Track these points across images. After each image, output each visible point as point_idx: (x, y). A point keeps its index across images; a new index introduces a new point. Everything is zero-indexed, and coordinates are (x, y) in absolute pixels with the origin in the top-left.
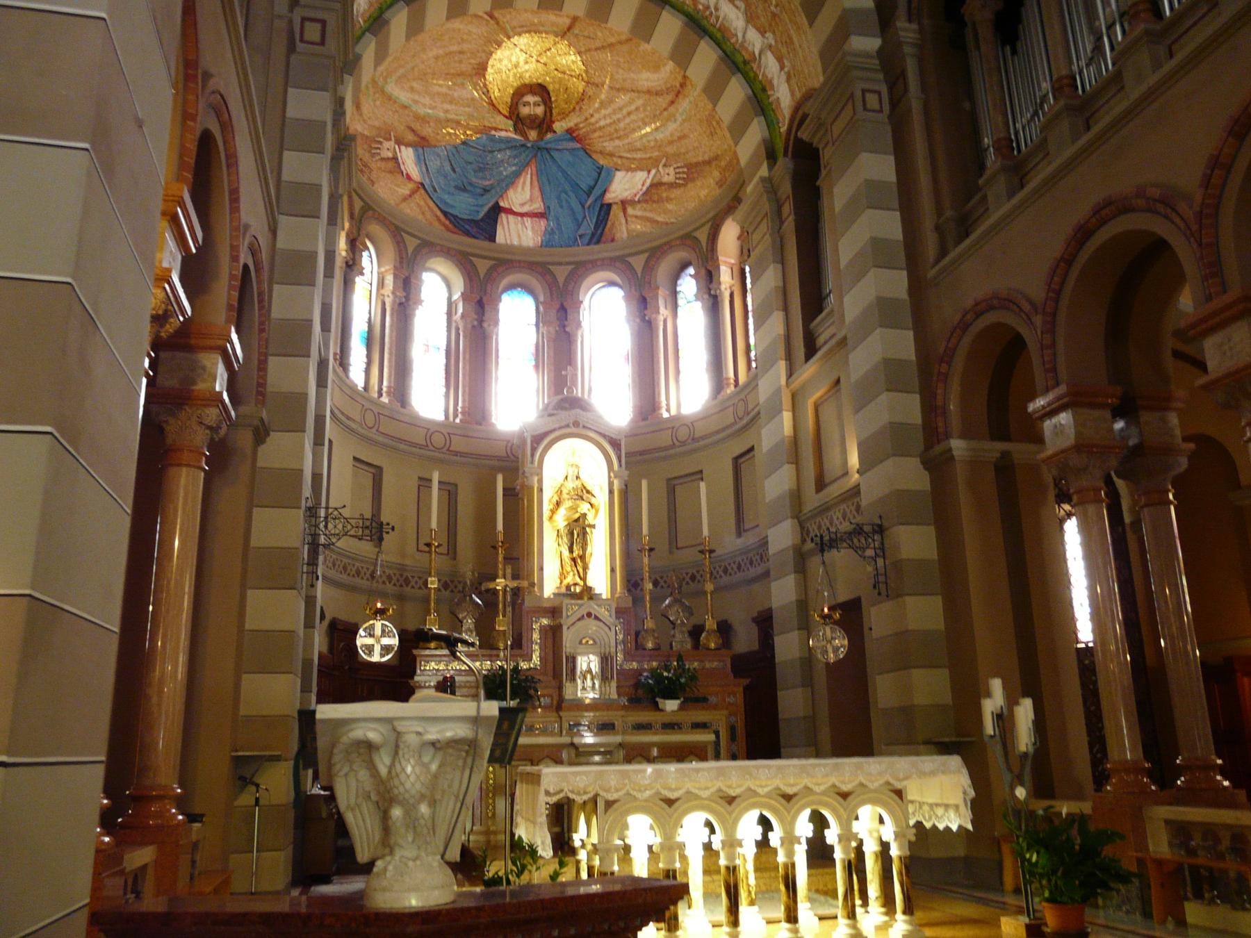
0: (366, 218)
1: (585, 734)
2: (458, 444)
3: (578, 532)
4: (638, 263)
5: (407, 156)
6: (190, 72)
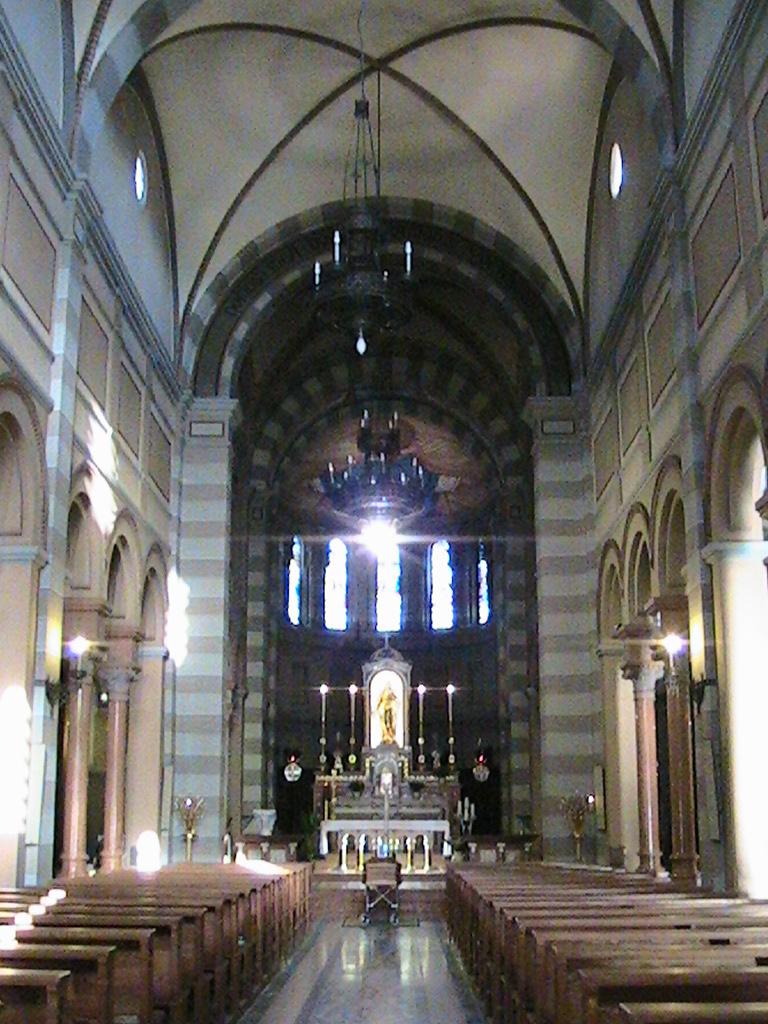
3: (388, 718)
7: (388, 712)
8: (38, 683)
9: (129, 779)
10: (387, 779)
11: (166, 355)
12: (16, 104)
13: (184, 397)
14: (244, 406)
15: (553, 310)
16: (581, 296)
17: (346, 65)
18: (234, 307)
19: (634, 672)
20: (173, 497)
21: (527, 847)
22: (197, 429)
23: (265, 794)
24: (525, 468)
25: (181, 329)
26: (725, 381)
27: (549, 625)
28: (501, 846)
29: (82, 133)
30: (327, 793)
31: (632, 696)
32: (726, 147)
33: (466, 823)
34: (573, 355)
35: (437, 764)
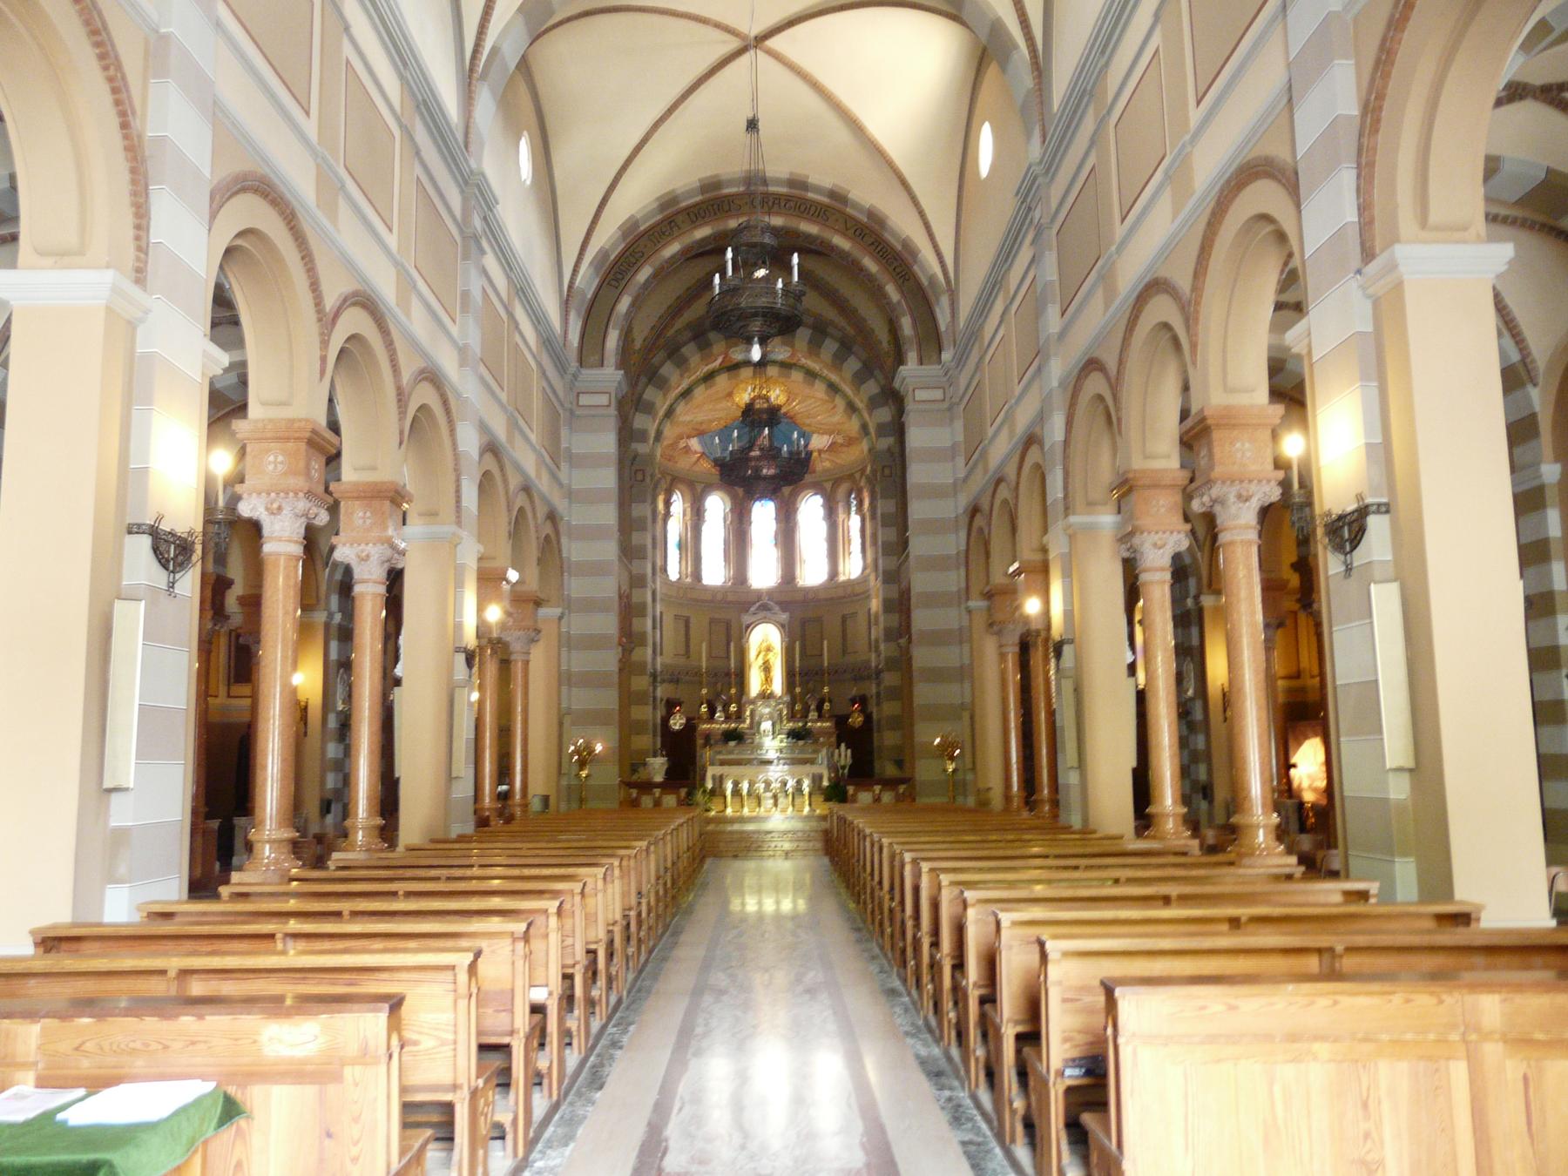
0: (674, 481)
1: (616, 888)
2: (730, 598)
3: (767, 668)
4: (828, 485)
5: (694, 444)
6: (504, 788)
9: (556, 734)
15: (925, 282)
16: (952, 275)
17: (724, 42)
18: (617, 280)
21: (902, 788)
25: (566, 305)
28: (877, 788)
33: (843, 768)
34: (943, 328)
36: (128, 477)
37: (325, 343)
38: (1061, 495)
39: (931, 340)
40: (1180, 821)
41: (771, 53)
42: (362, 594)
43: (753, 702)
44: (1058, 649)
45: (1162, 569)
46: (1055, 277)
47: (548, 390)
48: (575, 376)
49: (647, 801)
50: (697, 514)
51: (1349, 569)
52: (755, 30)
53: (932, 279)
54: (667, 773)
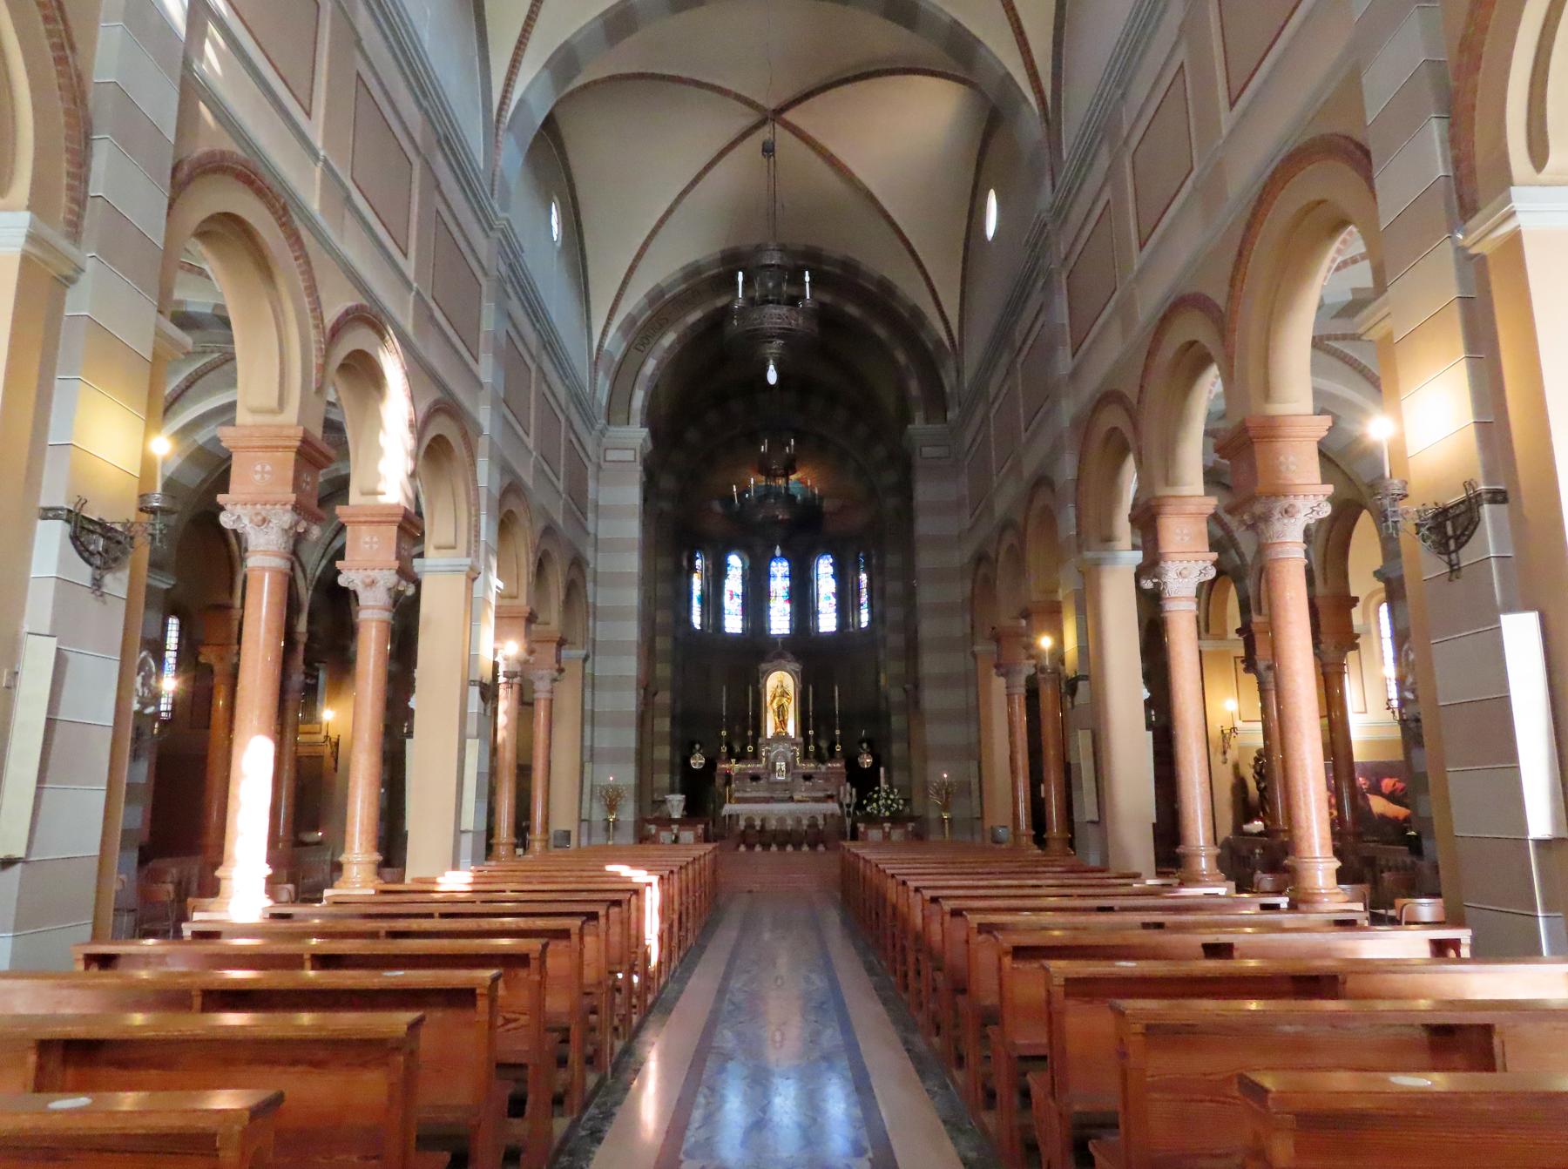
3: (781, 712)
7: (781, 706)
8: (472, 683)
10: (781, 765)
11: (582, 388)
12: (439, 141)
13: (598, 427)
14: (654, 435)
19: (1004, 669)
20: (590, 516)
21: (910, 826)
22: (612, 455)
23: (672, 783)
24: (905, 490)
25: (595, 365)
26: (1099, 401)
27: (928, 628)
29: (502, 176)
30: (728, 779)
31: (1004, 691)
32: (1103, 185)
34: (948, 389)
35: (825, 752)
36: (472, 659)
37: (327, 354)
38: (1073, 533)
39: (937, 401)
40: (1213, 861)
41: (789, 126)
42: (366, 620)
43: (769, 742)
44: (1072, 686)
45: (1187, 598)
46: (1066, 321)
47: (513, 334)
48: (602, 433)
49: (665, 836)
50: (717, 575)
51: (1454, 569)
52: (772, 105)
53: (939, 343)
54: (686, 808)
